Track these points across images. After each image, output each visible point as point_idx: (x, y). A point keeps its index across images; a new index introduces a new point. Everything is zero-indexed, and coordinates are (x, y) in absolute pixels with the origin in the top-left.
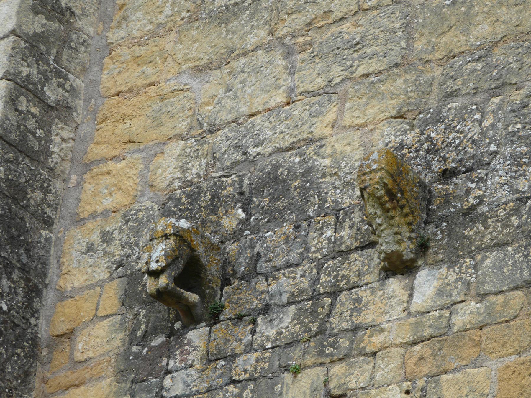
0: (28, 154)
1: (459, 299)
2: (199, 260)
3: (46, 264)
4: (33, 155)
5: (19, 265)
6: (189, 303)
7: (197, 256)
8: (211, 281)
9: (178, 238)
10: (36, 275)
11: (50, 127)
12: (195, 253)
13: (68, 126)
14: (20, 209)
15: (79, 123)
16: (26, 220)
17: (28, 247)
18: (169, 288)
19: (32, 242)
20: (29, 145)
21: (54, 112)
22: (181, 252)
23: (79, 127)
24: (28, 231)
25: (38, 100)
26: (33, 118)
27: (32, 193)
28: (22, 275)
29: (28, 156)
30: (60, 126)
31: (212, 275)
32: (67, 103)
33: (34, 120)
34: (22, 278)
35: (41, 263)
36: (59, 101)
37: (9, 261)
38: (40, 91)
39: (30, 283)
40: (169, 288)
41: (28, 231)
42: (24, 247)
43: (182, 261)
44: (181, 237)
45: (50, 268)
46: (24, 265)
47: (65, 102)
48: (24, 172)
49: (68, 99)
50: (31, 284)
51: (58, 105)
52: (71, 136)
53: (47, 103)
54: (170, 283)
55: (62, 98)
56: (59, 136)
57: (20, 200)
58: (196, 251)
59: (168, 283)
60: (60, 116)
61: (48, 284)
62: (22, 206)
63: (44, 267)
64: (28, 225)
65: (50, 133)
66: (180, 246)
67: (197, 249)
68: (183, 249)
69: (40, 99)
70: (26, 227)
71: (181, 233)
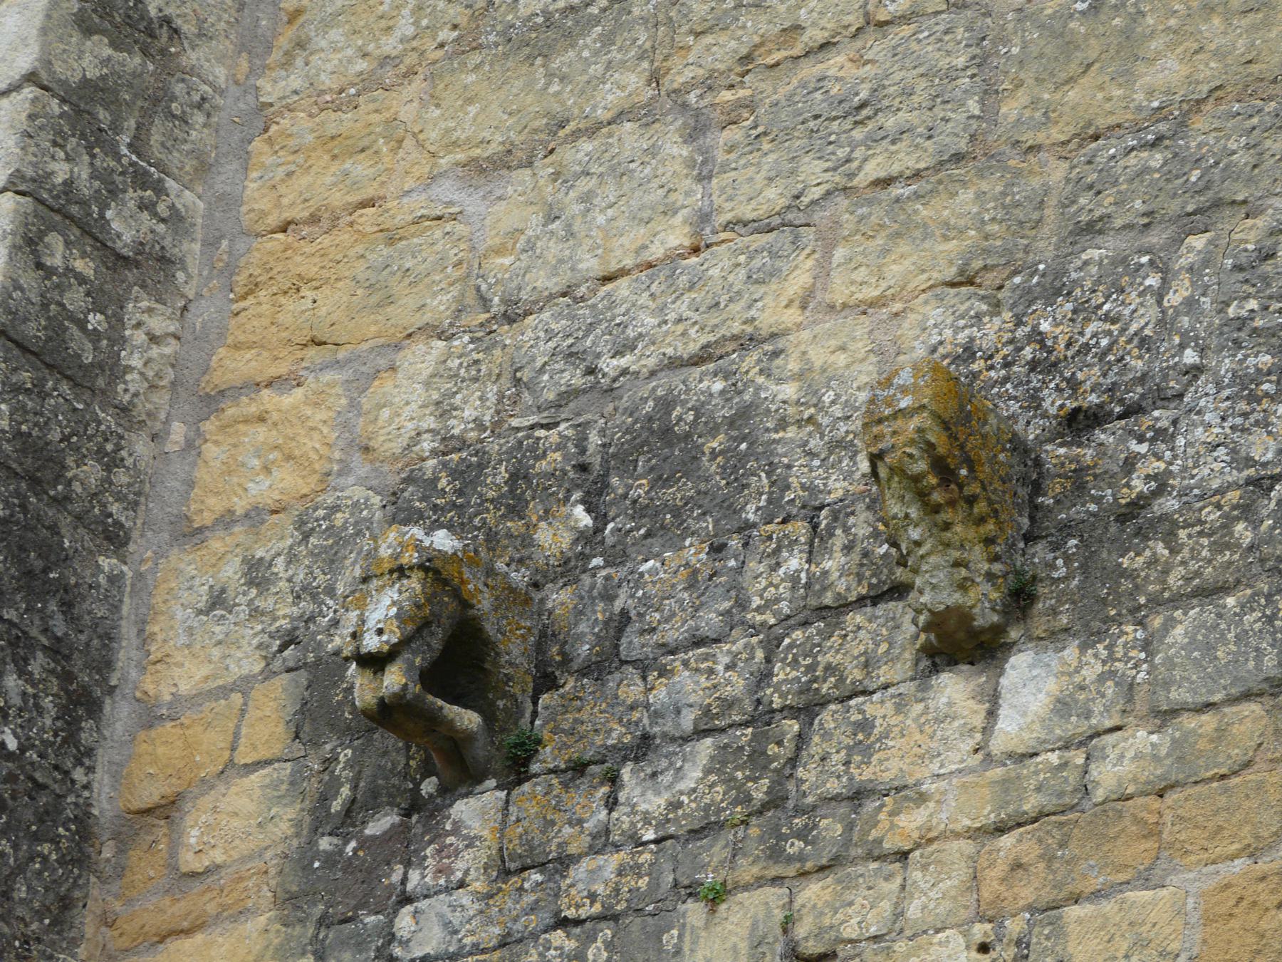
0: (69, 373)
1: (1108, 724)
2: (481, 630)
3: (110, 639)
4: (81, 374)
5: (45, 641)
6: (457, 731)
7: (475, 618)
8: (509, 680)
9: (430, 575)
10: (87, 666)
11: (122, 308)
12: (471, 612)
13: (165, 304)
14: (47, 505)
15: (191, 297)
16: (63, 531)
17: (67, 598)
18: (409, 697)
19: (77, 585)
20: (70, 351)
21: (130, 270)
22: (436, 608)
23: (192, 307)
24: (67, 558)
25: (91, 241)
26: (80, 285)
27: (78, 466)
28: (53, 665)
29: (68, 378)
30: (144, 304)
31: (511, 664)
32: (163, 248)
33: (81, 289)
34: (52, 672)
35: (100, 637)
36: (141, 244)
37: (23, 632)
38: (96, 220)
39: (72, 683)
40: (409, 697)
41: (67, 558)
42: (58, 596)
43: (440, 630)
44: (437, 572)
45: (121, 647)
46: (58, 639)
47: (157, 247)
48: (57, 416)
49: (163, 238)
50: (74, 686)
51: (140, 254)
52: (172, 329)
53: (113, 249)
54: (411, 685)
55: (150, 236)
56: (144, 328)
57: (48, 483)
58: (472, 607)
59: (406, 685)
60: (144, 281)
61: (115, 687)
62: (54, 499)
63: (105, 645)
64: (67, 544)
65: (121, 320)
66: (434, 595)
67: (475, 601)
68: (441, 603)
69: (96, 239)
70: (64, 549)
71: (438, 564)
